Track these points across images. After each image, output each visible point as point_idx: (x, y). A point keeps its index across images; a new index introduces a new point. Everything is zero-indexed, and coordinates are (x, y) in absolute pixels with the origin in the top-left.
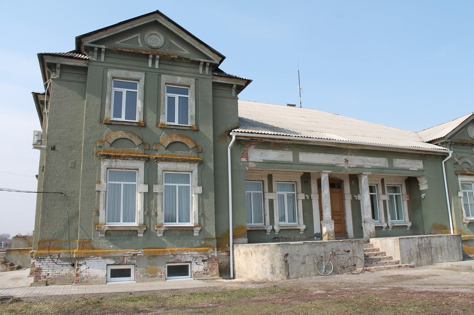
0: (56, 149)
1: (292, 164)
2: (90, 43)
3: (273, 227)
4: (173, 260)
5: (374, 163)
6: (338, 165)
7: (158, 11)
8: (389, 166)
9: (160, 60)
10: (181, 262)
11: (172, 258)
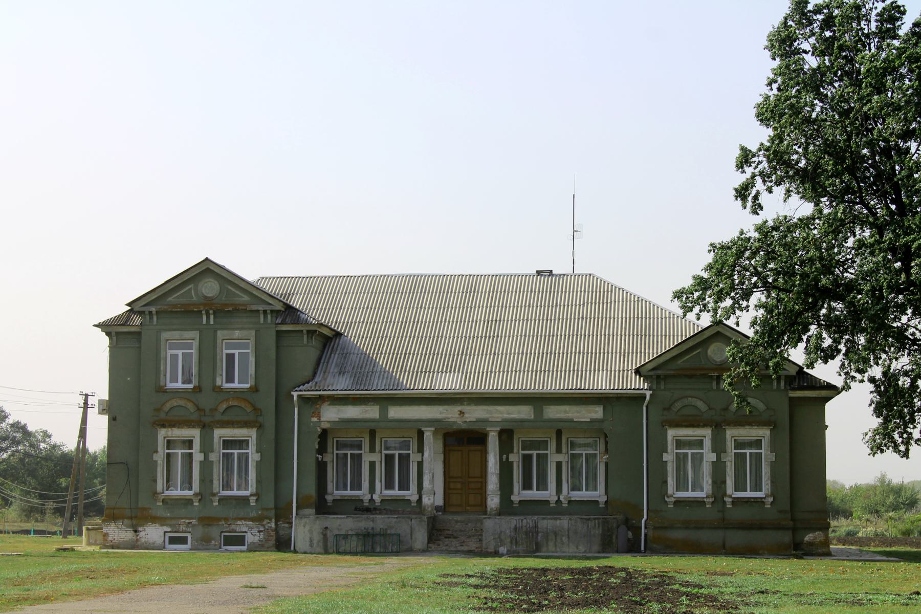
0: (117, 419)
1: (379, 422)
2: (141, 307)
3: (372, 497)
4: (228, 529)
5: (508, 414)
6: (447, 420)
7: (207, 259)
8: (535, 416)
9: (214, 313)
10: (236, 532)
11: (227, 528)
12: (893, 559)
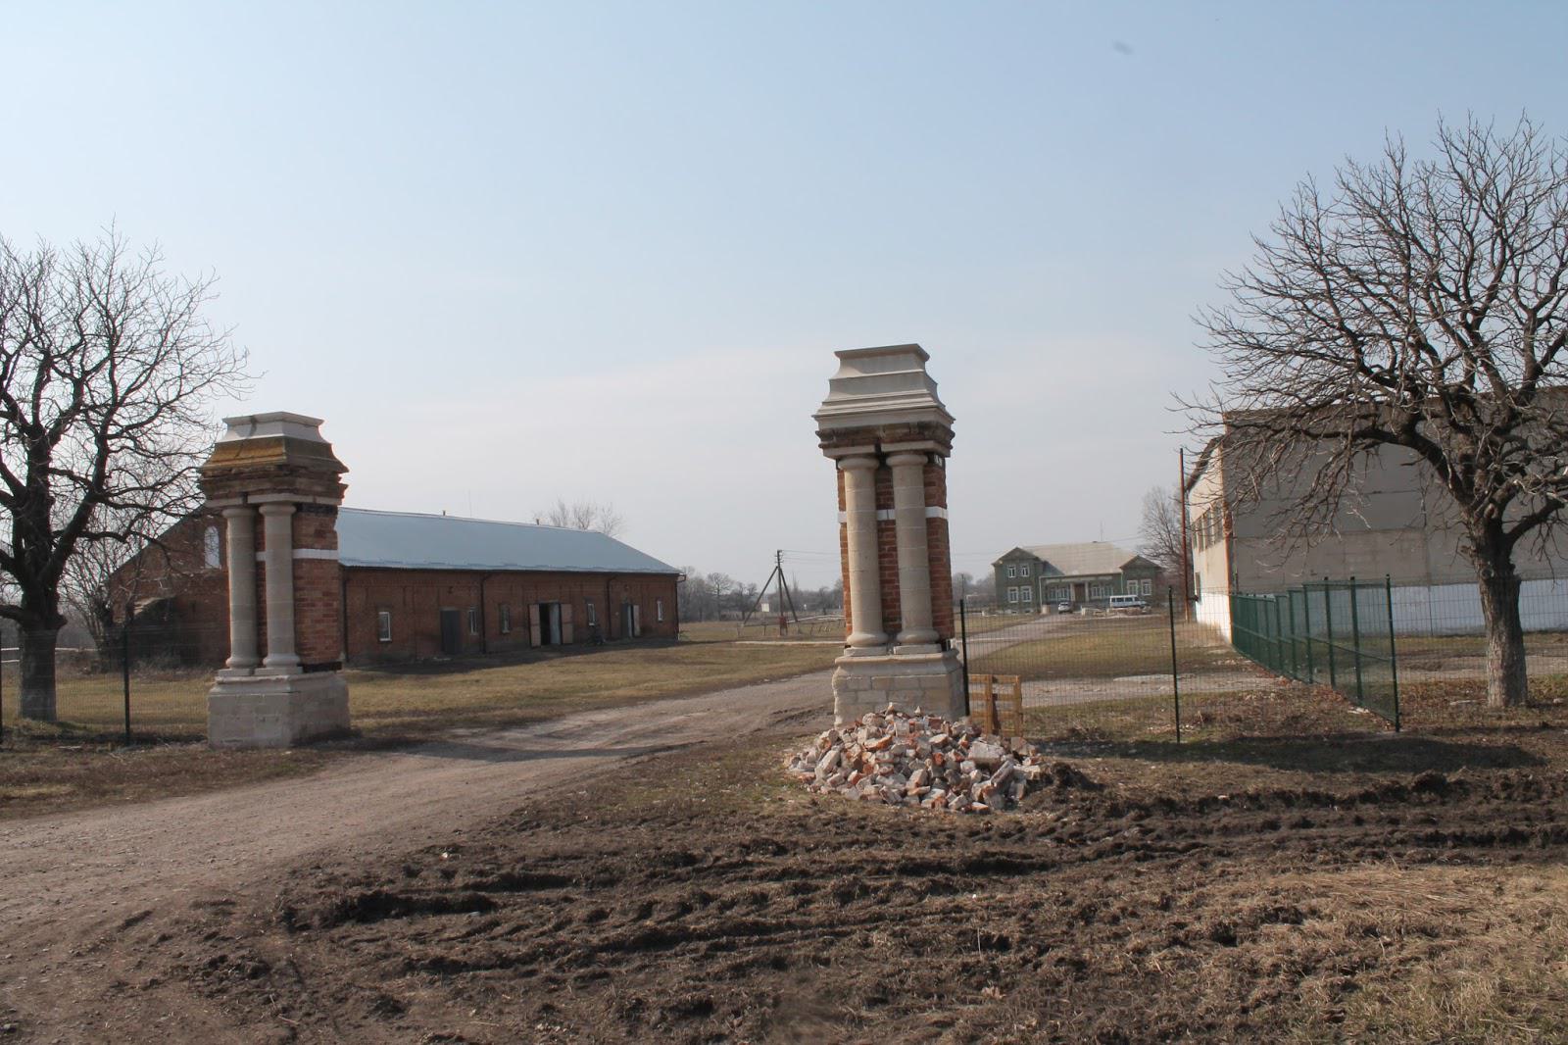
12: (1465, 740)
